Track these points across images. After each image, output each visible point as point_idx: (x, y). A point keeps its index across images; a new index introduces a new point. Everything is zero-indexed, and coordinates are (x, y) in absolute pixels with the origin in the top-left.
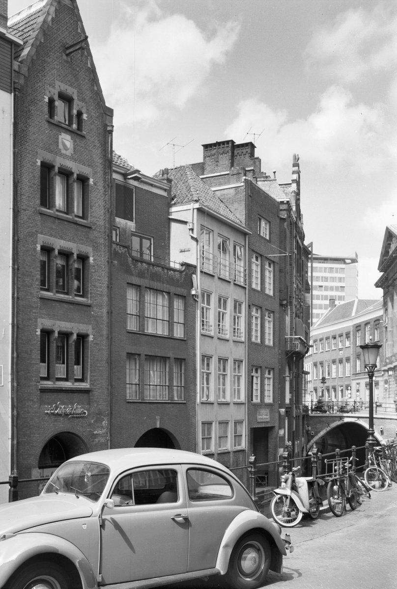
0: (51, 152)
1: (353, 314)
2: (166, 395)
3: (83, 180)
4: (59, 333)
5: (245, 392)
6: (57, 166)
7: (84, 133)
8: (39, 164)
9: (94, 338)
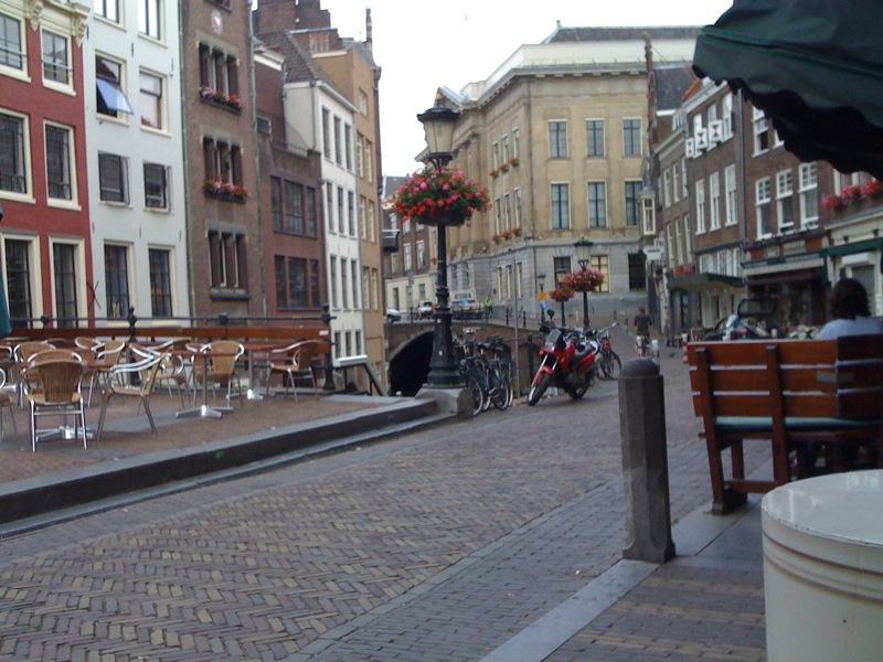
0: (207, 32)
1: (68, 89)
2: (102, 438)
3: (231, 60)
4: (223, 234)
5: (215, 482)
6: (211, 48)
7: (230, 9)
8: (197, 46)
9: (250, 239)
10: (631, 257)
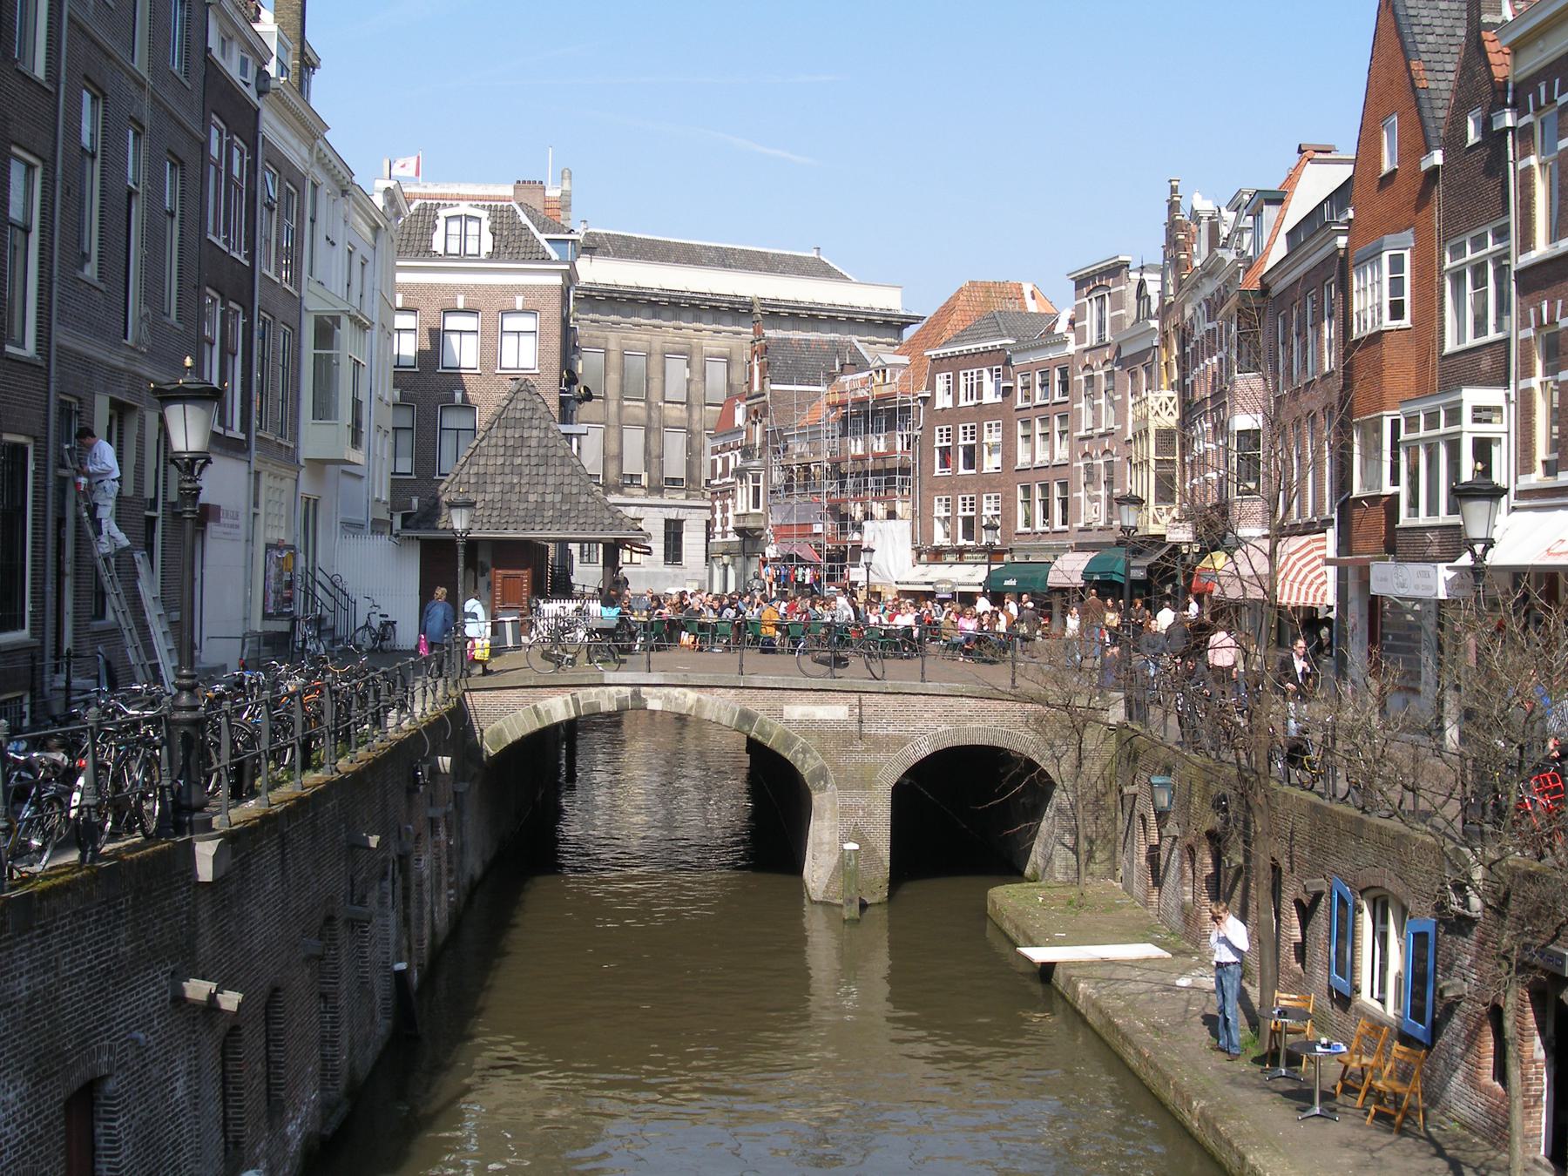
10: (668, 522)
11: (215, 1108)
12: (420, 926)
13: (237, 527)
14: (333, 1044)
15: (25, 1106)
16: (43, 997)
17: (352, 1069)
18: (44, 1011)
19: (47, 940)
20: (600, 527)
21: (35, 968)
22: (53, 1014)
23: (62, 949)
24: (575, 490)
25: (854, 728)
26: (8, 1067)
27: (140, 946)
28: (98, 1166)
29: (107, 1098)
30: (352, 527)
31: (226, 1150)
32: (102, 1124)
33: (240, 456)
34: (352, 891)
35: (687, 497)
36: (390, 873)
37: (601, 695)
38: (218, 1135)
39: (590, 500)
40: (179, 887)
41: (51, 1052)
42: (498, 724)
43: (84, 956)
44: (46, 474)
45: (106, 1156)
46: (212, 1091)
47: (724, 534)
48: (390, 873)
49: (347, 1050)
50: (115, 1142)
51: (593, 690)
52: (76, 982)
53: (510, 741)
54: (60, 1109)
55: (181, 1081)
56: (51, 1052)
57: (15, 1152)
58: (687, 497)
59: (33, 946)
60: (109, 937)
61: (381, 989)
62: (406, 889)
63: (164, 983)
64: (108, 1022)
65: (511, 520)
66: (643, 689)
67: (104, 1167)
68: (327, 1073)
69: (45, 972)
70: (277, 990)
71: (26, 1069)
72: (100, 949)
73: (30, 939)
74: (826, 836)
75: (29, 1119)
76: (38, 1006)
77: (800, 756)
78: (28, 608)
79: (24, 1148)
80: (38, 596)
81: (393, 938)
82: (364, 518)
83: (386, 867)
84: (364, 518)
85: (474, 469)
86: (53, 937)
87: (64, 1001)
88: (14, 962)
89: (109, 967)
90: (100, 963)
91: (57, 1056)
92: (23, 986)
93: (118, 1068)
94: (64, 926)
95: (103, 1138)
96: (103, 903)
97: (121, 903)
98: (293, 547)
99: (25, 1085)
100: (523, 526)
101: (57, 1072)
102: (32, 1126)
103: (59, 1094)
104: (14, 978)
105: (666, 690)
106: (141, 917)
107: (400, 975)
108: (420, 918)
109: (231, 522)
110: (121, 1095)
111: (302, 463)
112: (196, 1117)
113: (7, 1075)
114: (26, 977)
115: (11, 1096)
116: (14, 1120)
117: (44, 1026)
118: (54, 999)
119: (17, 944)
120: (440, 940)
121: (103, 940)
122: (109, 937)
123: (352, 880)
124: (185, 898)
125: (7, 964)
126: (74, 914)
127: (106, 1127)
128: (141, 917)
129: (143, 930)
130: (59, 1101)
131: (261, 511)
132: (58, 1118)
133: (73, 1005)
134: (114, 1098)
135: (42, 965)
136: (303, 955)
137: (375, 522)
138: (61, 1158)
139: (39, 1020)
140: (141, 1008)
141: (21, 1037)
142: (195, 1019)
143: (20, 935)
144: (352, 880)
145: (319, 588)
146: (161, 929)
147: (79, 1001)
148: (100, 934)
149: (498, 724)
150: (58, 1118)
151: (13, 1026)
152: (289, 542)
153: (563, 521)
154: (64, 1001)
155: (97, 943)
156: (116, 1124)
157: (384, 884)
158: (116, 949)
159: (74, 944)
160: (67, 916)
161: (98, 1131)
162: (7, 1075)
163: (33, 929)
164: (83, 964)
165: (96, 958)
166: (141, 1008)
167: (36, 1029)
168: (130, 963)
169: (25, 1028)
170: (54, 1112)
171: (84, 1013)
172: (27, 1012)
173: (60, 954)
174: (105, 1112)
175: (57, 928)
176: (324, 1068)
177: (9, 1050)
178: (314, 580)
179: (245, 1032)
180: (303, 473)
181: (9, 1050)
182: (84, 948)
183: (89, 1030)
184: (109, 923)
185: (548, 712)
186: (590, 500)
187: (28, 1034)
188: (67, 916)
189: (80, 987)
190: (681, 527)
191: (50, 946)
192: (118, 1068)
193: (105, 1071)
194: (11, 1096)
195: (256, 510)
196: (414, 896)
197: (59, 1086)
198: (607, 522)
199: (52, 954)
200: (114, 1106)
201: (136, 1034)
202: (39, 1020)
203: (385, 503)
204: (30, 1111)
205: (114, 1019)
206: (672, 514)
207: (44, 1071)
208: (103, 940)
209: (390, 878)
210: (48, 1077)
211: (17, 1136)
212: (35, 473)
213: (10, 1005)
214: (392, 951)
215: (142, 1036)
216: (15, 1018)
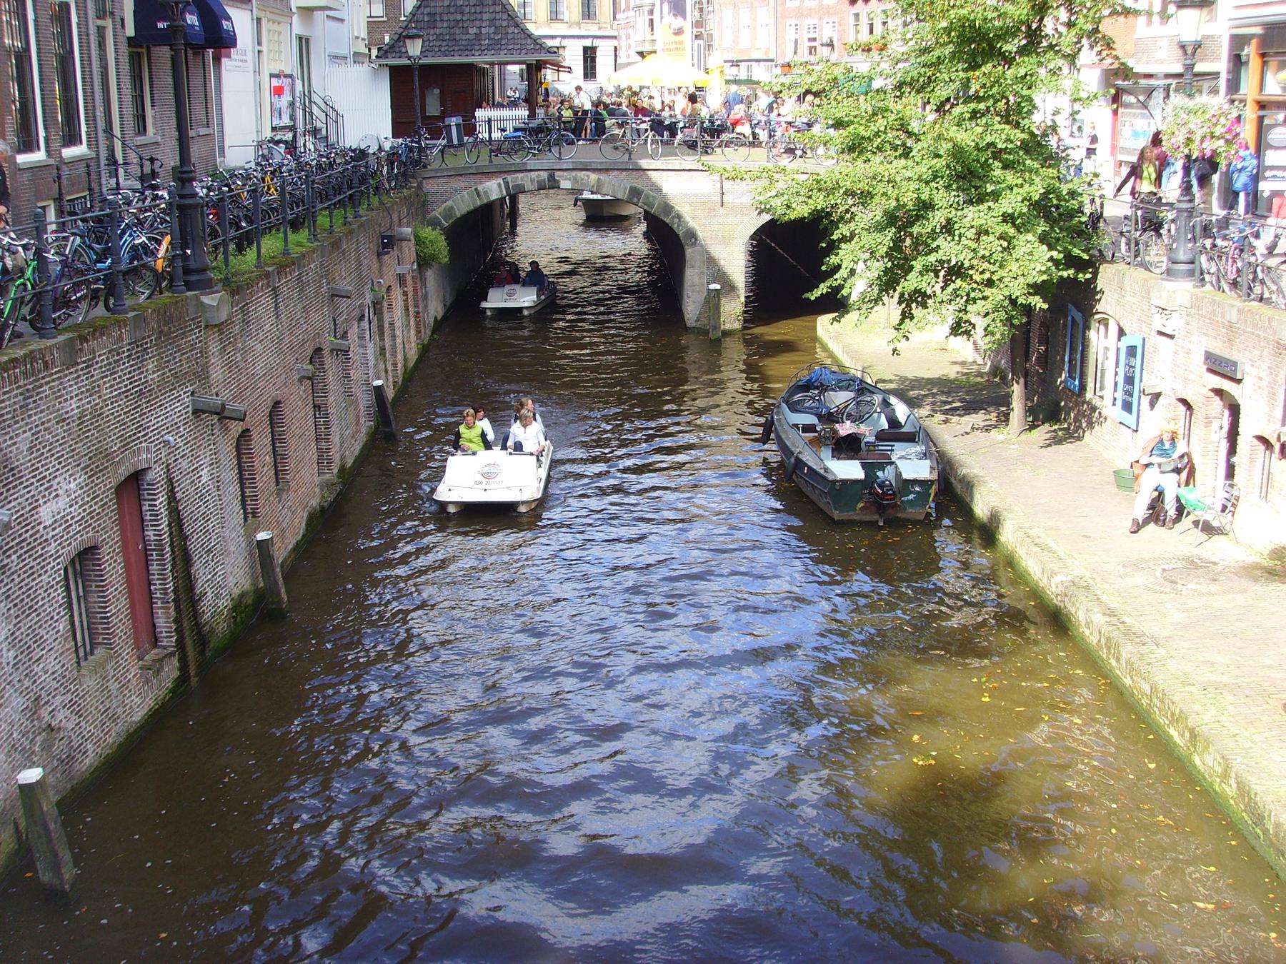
10: (586, 49)
11: (234, 489)
12: (394, 354)
13: (246, 61)
14: (327, 440)
15: (84, 492)
16: (91, 413)
17: (343, 458)
18: (92, 424)
19: (90, 372)
20: (524, 52)
21: (82, 393)
22: (100, 425)
23: (103, 378)
24: (504, 24)
25: (717, 198)
26: (68, 464)
27: (164, 374)
28: (146, 533)
29: (148, 485)
30: (337, 58)
31: (246, 519)
32: (147, 503)
33: (245, 6)
34: (335, 329)
35: (600, 28)
36: (367, 315)
37: (525, 178)
38: (238, 508)
39: (516, 31)
40: (193, 330)
41: (101, 453)
42: (449, 203)
43: (120, 383)
44: (87, 25)
45: (152, 526)
46: (230, 476)
47: (628, 56)
48: (367, 315)
49: (338, 445)
50: (157, 515)
51: (520, 175)
52: (116, 402)
53: (459, 216)
54: (112, 494)
55: (206, 470)
56: (101, 453)
57: (80, 525)
58: (600, 28)
59: (79, 376)
60: (139, 368)
61: (364, 400)
62: (381, 328)
63: (186, 400)
64: (144, 429)
65: (457, 48)
66: (557, 173)
67: (151, 533)
68: (323, 461)
69: (90, 396)
70: (278, 402)
71: (82, 465)
72: (133, 377)
73: (76, 371)
74: (696, 279)
75: (88, 502)
76: (88, 420)
77: (676, 220)
78: (84, 128)
79: (86, 522)
80: (91, 119)
81: (371, 363)
82: (347, 52)
83: (363, 310)
84: (347, 52)
85: (427, 10)
86: (95, 370)
87: (108, 416)
88: (64, 389)
89: (141, 390)
90: (134, 388)
91: (106, 456)
92: (74, 406)
93: (155, 462)
94: (103, 360)
95: (149, 513)
96: (132, 343)
97: (147, 343)
98: (291, 76)
99: (83, 477)
100: (467, 52)
101: (107, 467)
102: (91, 506)
103: (110, 482)
104: (66, 400)
105: (574, 174)
106: (164, 352)
107: (378, 390)
108: (394, 347)
109: (241, 58)
110: (159, 482)
111: (294, 10)
112: (219, 495)
113: (68, 470)
114: (75, 399)
115: (72, 485)
116: (77, 503)
117: (93, 434)
118: (99, 415)
119: (66, 376)
120: (411, 364)
121: (134, 370)
122: (139, 368)
123: (334, 320)
124: (197, 338)
125: (59, 391)
126: (110, 352)
127: (150, 505)
128: (164, 352)
129: (165, 362)
130: (111, 488)
131: (264, 48)
132: (111, 500)
133: (115, 418)
134: (154, 485)
135: (88, 390)
136: (298, 376)
137: (356, 54)
138: (115, 529)
139: (90, 430)
140: (169, 419)
141: (76, 443)
142: (212, 425)
143: (67, 369)
144: (334, 320)
145: (314, 107)
146: (180, 361)
147: (120, 415)
148: (131, 366)
149: (449, 203)
150: (111, 500)
151: (69, 435)
152: (288, 72)
153: (496, 48)
154: (108, 416)
155: (130, 373)
156: (157, 503)
157: (362, 323)
158: (145, 377)
159: (111, 374)
160: (104, 354)
161: (144, 508)
162: (68, 470)
163: (78, 364)
164: (120, 388)
165: (131, 383)
166: (169, 419)
167: (87, 437)
168: (158, 386)
169: (79, 436)
170: (107, 496)
171: (124, 424)
172: (79, 425)
173: (101, 382)
174: (148, 494)
175: (97, 363)
176: (320, 457)
177: (67, 453)
178: (310, 101)
179: (254, 434)
180: (295, 18)
181: (67, 453)
182: (120, 377)
183: (130, 436)
184: (138, 358)
185: (486, 192)
186: (516, 31)
187: (82, 440)
188: (104, 354)
189: (119, 405)
190: (595, 53)
191: (92, 376)
192: (155, 462)
193: (144, 465)
194: (72, 485)
195: (260, 48)
196: (387, 333)
197: (109, 477)
198: (529, 47)
199: (94, 382)
200: (154, 490)
201: (166, 437)
202: (90, 430)
203: (363, 39)
204: (88, 496)
205: (149, 427)
206: (588, 43)
207: (97, 467)
208: (134, 370)
209: (366, 318)
210: (100, 471)
211: (80, 514)
212: (78, 24)
213: (64, 420)
214: (371, 372)
215: (171, 439)
216: (70, 429)
